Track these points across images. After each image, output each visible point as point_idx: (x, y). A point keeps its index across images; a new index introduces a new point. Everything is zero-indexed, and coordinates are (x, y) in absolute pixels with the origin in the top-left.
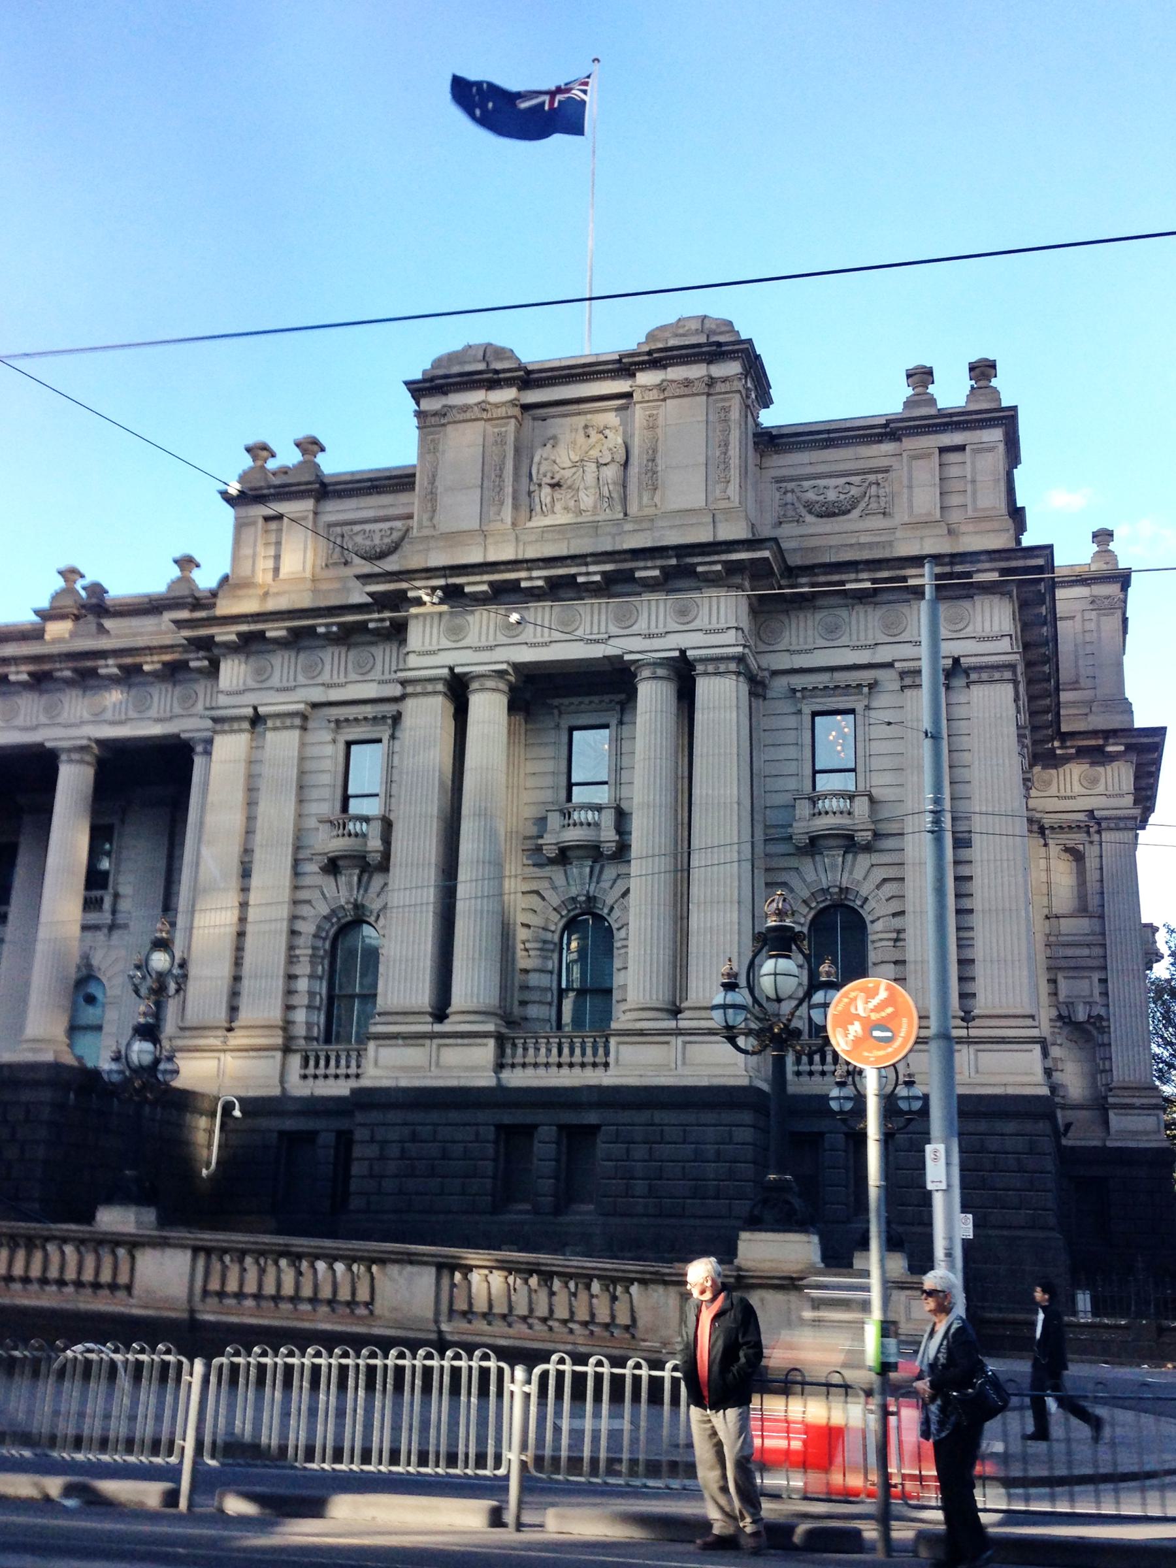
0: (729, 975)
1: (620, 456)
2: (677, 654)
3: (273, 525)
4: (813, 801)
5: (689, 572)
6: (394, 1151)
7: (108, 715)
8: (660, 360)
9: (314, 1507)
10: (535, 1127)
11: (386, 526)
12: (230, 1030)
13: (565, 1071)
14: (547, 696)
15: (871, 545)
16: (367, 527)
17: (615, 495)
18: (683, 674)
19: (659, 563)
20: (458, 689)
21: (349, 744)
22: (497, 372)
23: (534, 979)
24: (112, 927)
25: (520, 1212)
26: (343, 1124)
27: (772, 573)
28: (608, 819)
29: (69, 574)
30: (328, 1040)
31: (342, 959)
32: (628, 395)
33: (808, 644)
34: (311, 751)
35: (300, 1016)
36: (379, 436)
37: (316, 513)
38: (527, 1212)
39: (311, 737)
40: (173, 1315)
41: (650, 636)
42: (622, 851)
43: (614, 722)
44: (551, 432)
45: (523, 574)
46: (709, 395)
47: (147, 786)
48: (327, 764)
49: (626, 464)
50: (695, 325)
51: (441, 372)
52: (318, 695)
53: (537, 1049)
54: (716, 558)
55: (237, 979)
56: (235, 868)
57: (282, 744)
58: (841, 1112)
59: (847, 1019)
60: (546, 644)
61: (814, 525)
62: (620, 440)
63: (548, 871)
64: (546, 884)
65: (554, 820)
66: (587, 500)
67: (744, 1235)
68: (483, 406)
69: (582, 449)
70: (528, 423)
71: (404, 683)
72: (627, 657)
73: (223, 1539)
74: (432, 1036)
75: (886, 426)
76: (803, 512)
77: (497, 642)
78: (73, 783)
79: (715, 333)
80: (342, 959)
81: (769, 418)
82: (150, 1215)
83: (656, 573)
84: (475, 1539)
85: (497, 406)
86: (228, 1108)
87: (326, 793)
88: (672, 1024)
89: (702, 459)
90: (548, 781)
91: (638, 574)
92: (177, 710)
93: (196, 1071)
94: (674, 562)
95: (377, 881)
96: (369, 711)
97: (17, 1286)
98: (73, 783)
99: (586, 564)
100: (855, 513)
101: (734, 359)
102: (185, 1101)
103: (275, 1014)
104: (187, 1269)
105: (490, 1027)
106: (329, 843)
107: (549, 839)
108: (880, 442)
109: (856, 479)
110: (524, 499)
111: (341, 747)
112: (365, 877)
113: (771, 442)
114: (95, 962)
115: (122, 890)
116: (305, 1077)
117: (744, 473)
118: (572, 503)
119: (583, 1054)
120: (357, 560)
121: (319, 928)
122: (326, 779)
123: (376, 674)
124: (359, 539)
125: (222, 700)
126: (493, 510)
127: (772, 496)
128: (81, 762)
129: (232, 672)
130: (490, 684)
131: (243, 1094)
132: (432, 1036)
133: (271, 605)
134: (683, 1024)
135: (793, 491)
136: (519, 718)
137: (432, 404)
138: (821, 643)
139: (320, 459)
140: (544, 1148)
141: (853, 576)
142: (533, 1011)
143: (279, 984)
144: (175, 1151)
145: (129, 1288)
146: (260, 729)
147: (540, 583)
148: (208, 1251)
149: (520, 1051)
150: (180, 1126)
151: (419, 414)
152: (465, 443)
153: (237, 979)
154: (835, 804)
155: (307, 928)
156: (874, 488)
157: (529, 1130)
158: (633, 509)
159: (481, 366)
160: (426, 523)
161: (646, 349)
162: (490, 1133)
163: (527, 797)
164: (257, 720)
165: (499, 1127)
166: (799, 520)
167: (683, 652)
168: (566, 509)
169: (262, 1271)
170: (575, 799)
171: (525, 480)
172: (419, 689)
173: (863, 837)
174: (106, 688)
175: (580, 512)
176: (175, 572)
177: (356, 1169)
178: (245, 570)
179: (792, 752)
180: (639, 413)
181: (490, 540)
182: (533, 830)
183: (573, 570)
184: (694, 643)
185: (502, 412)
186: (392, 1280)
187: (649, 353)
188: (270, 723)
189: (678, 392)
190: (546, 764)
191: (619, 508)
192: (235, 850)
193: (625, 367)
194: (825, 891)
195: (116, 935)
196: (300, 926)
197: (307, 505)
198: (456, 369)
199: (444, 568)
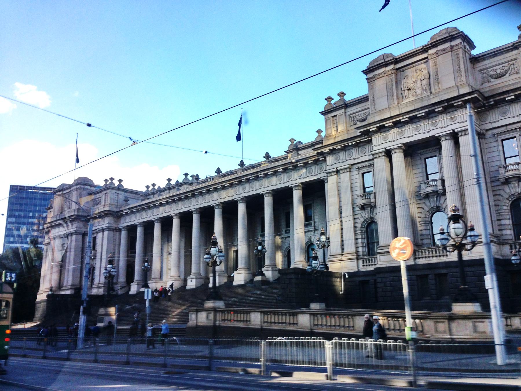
0: (441, 230)
1: (427, 76)
2: (452, 131)
3: (335, 118)
4: (505, 167)
5: (452, 106)
6: (388, 284)
7: (302, 176)
8: (435, 45)
9: (289, 374)
10: (428, 275)
11: (364, 111)
12: (343, 255)
13: (435, 258)
14: (414, 151)
15: (513, 84)
16: (360, 113)
17: (427, 88)
18: (455, 137)
19: (441, 105)
20: (388, 153)
22: (387, 62)
23: (424, 232)
25: (427, 299)
27: (479, 100)
28: (439, 183)
29: (292, 140)
30: (369, 255)
31: (369, 231)
32: (427, 58)
33: (497, 119)
34: (353, 177)
35: (360, 249)
36: (356, 87)
37: (345, 113)
38: (429, 299)
39: (352, 174)
40: (308, 330)
41: (443, 128)
42: (444, 193)
43: (438, 155)
44: (405, 75)
45: (401, 118)
46: (452, 51)
47: (314, 192)
48: (358, 180)
49: (429, 78)
50: (444, 32)
51: (372, 66)
52: (353, 162)
53: (425, 253)
54: (459, 100)
55: (342, 241)
56: (337, 212)
57: (345, 177)
58: (516, 264)
59: (395, 248)
60: (411, 136)
61: (495, 82)
62: (426, 72)
63: (423, 201)
64: (424, 204)
65: (423, 186)
66: (419, 92)
67: (454, 304)
68: (384, 72)
69: (415, 77)
70: (399, 73)
71: (373, 155)
72: (436, 135)
73: (257, 380)
75: (513, 46)
76: (490, 78)
77: (395, 138)
78: (297, 195)
79: (451, 32)
80: (369, 231)
81: (474, 52)
82: (323, 305)
83: (441, 109)
84: (322, 382)
85: (389, 71)
86: (344, 275)
87: (358, 188)
89: (452, 71)
90: (421, 175)
91: (436, 110)
92: (319, 172)
93: (333, 267)
94: (446, 104)
95: (442, 199)
96: (366, 164)
98: (297, 195)
99: (420, 111)
100: (507, 75)
101: (458, 38)
102: (332, 275)
103: (353, 250)
104: (309, 319)
106: (361, 201)
107: (422, 191)
108: (512, 51)
110: (400, 96)
111: (361, 175)
112: (438, 198)
113: (475, 60)
114: (312, 240)
115: (316, 220)
116: (364, 266)
117: (466, 71)
118: (415, 93)
119: (440, 253)
120: (358, 123)
121: (362, 225)
122: (358, 184)
123: (367, 153)
124: (358, 117)
125: (328, 168)
126: (392, 101)
127: (479, 76)
128: (298, 189)
129: (330, 159)
130: (397, 151)
131: (348, 272)
133: (337, 140)
135: (485, 73)
136: (409, 159)
137: (371, 75)
138: (501, 118)
139: (345, 97)
140: (431, 281)
141: (508, 95)
142: (425, 241)
143: (353, 241)
144: (331, 288)
145: (297, 324)
146: (339, 174)
147: (407, 119)
149: (420, 254)
150: (332, 281)
151: (367, 79)
152: (381, 84)
153: (342, 241)
154: (512, 167)
155: (359, 225)
156: (512, 66)
157: (427, 276)
158: (433, 91)
159: (383, 61)
160: (373, 109)
161: (430, 43)
163: (415, 180)
164: (338, 172)
166: (489, 81)
167: (453, 130)
168: (413, 95)
169: (322, 319)
170: (507, 163)
171: (400, 90)
172: (377, 156)
174: (301, 169)
175: (417, 95)
176: (317, 134)
177: (380, 290)
178: (329, 132)
179: (496, 154)
180: (431, 62)
181: (391, 110)
182: (417, 190)
183: (416, 113)
184: (456, 127)
185: (390, 72)
187: (431, 44)
188: (341, 172)
189: (442, 53)
190: (419, 170)
191: (429, 91)
192: (337, 207)
193: (425, 50)
194: (513, 195)
195: (316, 232)
196: (357, 225)
198: (376, 64)
199: (379, 121)
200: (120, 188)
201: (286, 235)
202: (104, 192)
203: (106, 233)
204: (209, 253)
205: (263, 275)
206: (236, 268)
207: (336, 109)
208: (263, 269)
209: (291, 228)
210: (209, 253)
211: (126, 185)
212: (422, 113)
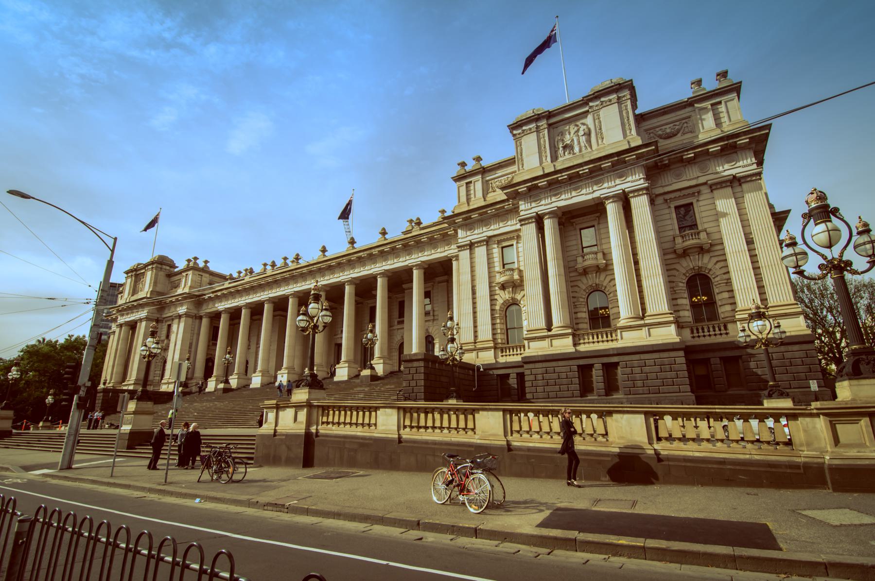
6: (540, 377)
13: (601, 344)
20: (539, 220)
21: (503, 248)
24: (434, 320)
26: (520, 370)
47: (439, 274)
74: (548, 337)
88: (642, 322)
97: (422, 430)
98: (416, 274)
100: (679, 135)
105: (570, 331)
109: (677, 123)
132: (548, 337)
134: (646, 322)
140: (597, 374)
148: (511, 412)
157: (590, 367)
162: (576, 368)
165: (579, 366)
173: (706, 247)
177: (528, 384)
179: (669, 222)
186: (616, 421)
197: (479, 177)
200: (205, 270)
201: (399, 326)
202: (184, 274)
203: (183, 319)
204: (306, 314)
205: (372, 368)
206: (279, 366)
207: (472, 174)
208: (372, 362)
209: (406, 319)
210: (306, 314)
211: (212, 267)
212: (586, 169)
